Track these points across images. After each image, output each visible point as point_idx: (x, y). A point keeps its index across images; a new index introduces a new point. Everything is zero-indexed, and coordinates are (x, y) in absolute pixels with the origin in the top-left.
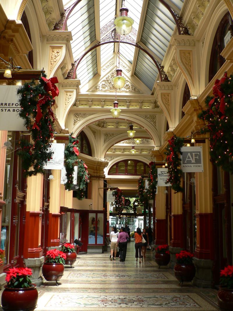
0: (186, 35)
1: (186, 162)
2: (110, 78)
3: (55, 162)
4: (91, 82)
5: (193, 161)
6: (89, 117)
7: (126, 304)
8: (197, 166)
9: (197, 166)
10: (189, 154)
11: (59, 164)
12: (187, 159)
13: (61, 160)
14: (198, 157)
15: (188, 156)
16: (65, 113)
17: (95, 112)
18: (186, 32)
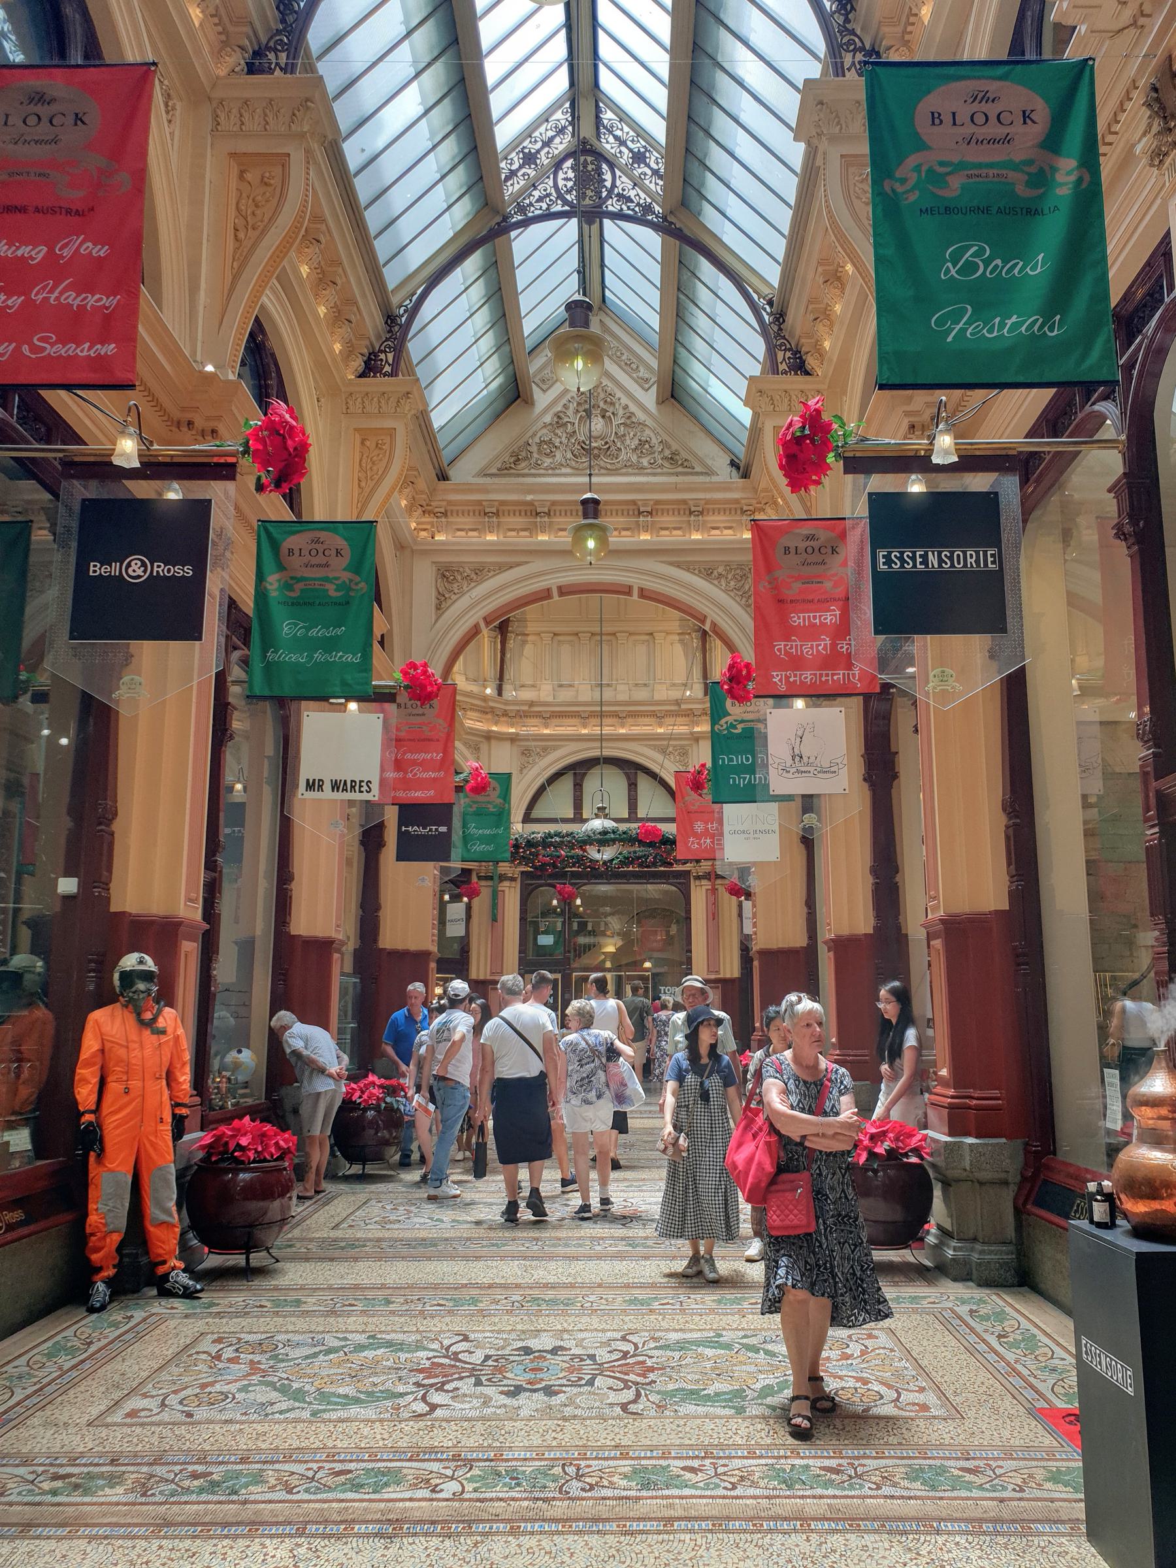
0: (796, 374)
2: (570, 412)
4: (439, 67)
6: (497, 577)
13: (839, 761)
17: (523, 559)
18: (799, 366)
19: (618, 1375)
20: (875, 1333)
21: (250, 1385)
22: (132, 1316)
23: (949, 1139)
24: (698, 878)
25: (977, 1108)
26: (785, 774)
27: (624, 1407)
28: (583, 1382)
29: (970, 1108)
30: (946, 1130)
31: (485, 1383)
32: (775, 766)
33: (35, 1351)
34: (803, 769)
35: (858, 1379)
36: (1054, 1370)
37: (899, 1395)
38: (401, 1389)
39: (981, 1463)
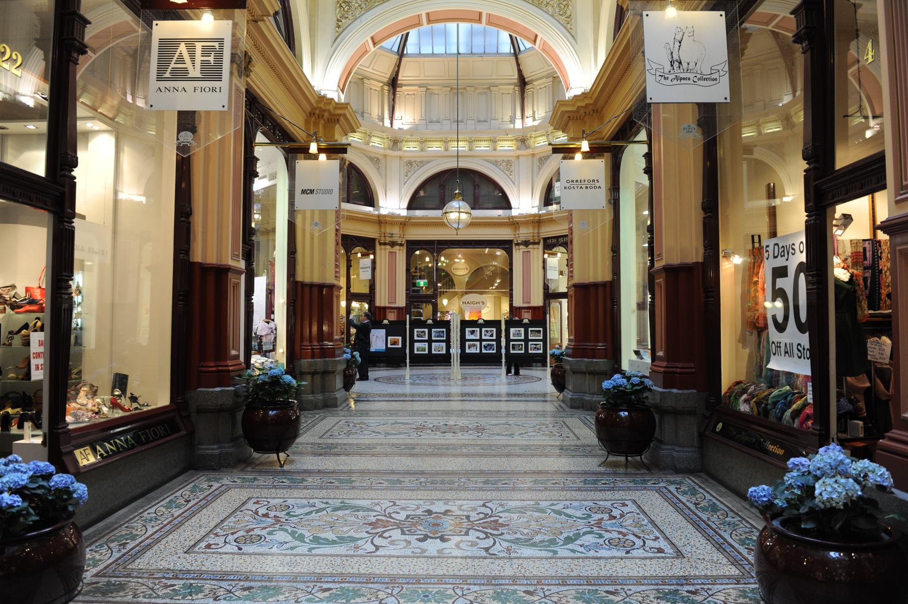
1: (167, 75)
3: (699, 76)
5: (195, 72)
7: (430, 512)
8: (207, 90)
9: (207, 90)
10: (183, 48)
11: (714, 82)
12: (172, 65)
13: (719, 67)
14: (211, 59)
15: (177, 54)
16: (292, 227)
19: (481, 529)
20: (626, 502)
21: (274, 531)
22: (212, 486)
23: (664, 390)
24: (518, 244)
25: (680, 373)
26: (663, 81)
27: (487, 550)
28: (463, 533)
29: (676, 373)
30: (661, 383)
31: (407, 533)
32: (653, 72)
33: (159, 505)
34: (682, 75)
35: (620, 533)
36: (729, 524)
37: (644, 543)
38: (357, 536)
39: (698, 587)
